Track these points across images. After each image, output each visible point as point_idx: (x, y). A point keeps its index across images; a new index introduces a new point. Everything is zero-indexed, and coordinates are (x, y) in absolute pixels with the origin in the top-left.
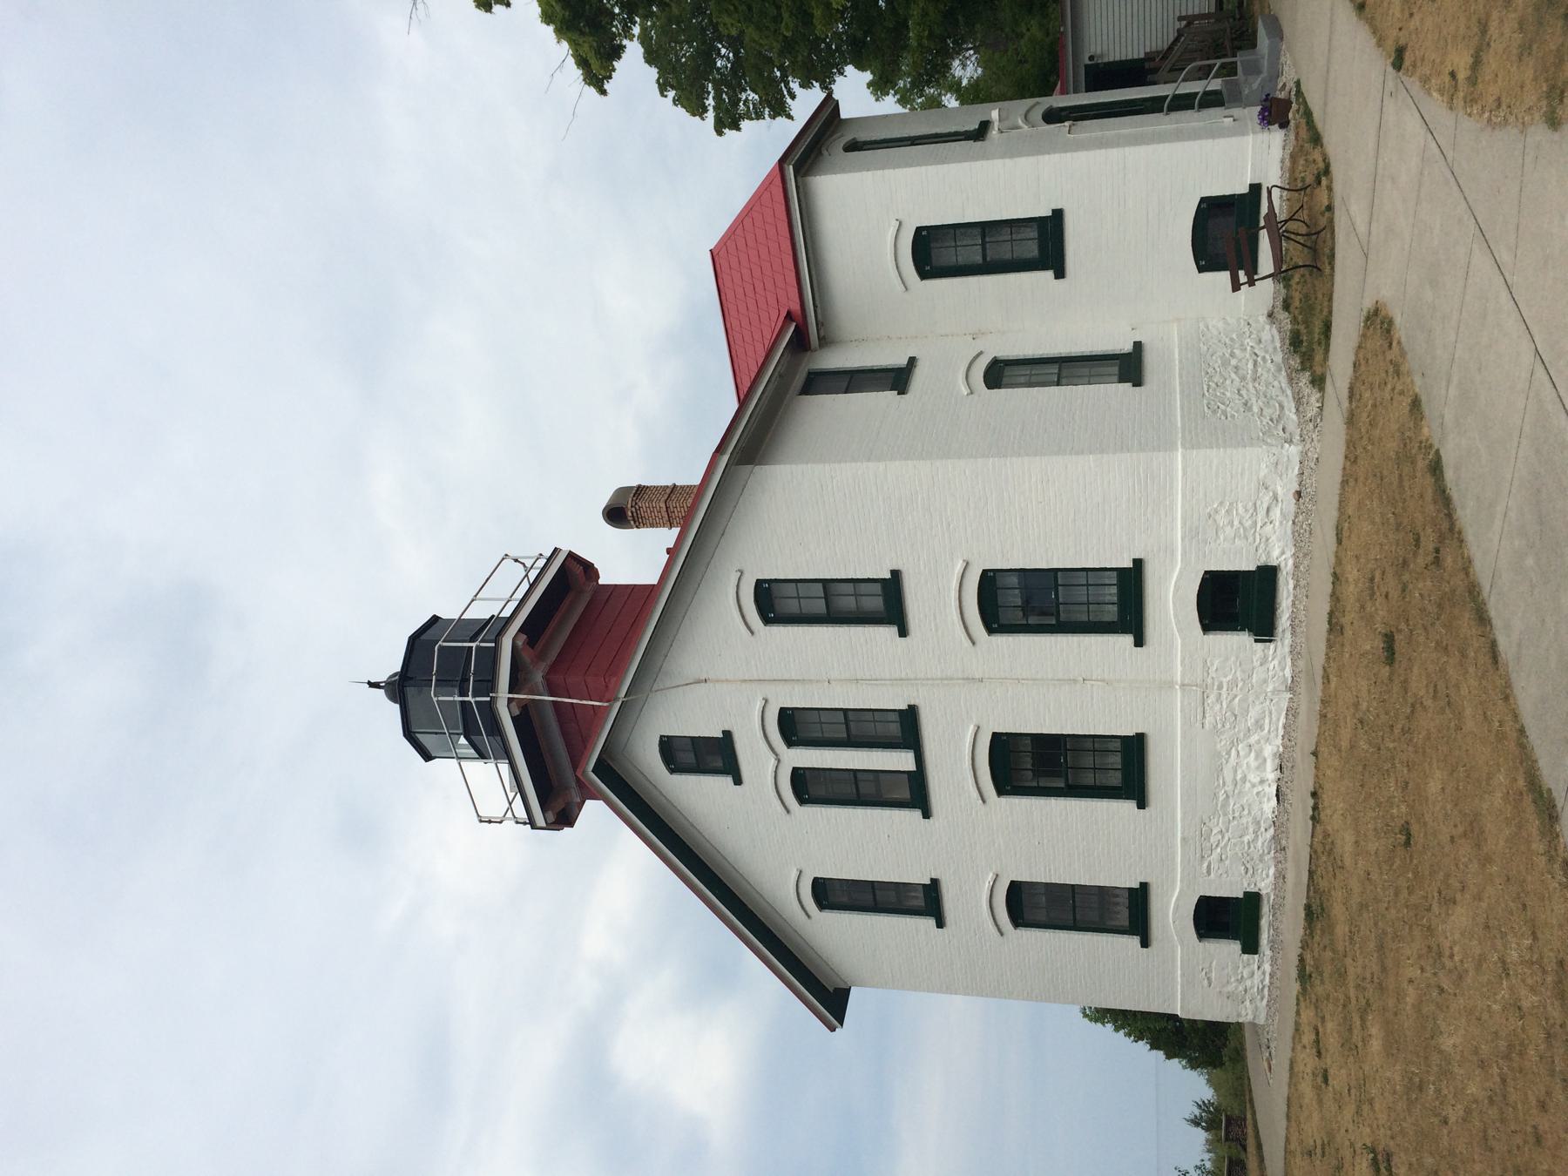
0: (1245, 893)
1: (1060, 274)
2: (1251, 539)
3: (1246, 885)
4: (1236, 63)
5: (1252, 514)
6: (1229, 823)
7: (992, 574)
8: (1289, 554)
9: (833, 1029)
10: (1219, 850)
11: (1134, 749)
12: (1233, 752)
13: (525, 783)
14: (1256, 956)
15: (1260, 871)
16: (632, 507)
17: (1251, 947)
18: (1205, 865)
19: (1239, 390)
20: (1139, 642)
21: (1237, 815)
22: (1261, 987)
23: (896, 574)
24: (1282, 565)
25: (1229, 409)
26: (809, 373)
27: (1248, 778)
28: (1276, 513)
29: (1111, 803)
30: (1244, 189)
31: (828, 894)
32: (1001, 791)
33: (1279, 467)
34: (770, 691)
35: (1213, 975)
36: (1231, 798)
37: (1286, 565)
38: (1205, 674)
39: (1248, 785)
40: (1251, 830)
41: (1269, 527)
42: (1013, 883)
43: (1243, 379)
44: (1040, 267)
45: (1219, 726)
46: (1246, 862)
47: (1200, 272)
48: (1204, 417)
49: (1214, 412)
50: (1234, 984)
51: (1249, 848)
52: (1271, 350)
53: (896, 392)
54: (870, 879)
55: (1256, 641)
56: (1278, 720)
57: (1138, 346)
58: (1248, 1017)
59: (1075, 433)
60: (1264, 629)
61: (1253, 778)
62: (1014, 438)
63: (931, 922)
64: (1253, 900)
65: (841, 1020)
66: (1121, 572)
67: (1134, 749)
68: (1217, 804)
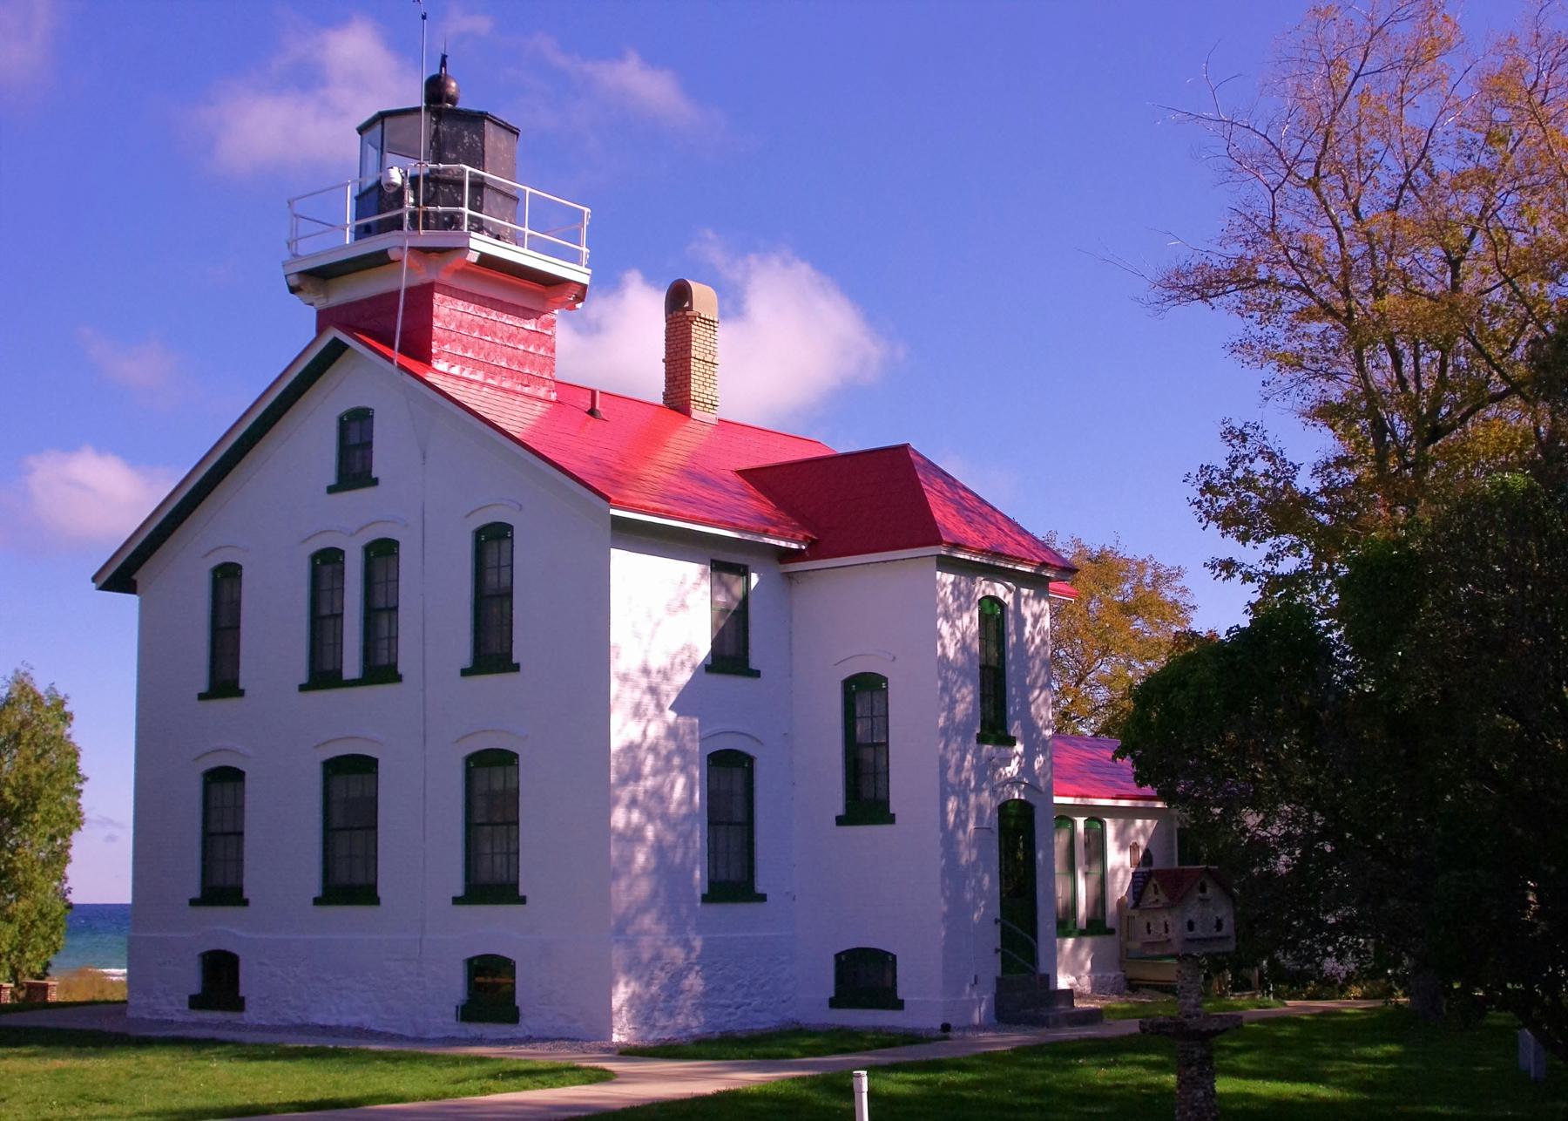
9: (94, 579)
13: (366, 349)
14: (187, 1008)
23: (375, 482)
30: (900, 996)
31: (227, 577)
54: (243, 625)
55: (457, 1007)
57: (762, 898)
64: (238, 1004)
65: (105, 587)
66: (516, 886)
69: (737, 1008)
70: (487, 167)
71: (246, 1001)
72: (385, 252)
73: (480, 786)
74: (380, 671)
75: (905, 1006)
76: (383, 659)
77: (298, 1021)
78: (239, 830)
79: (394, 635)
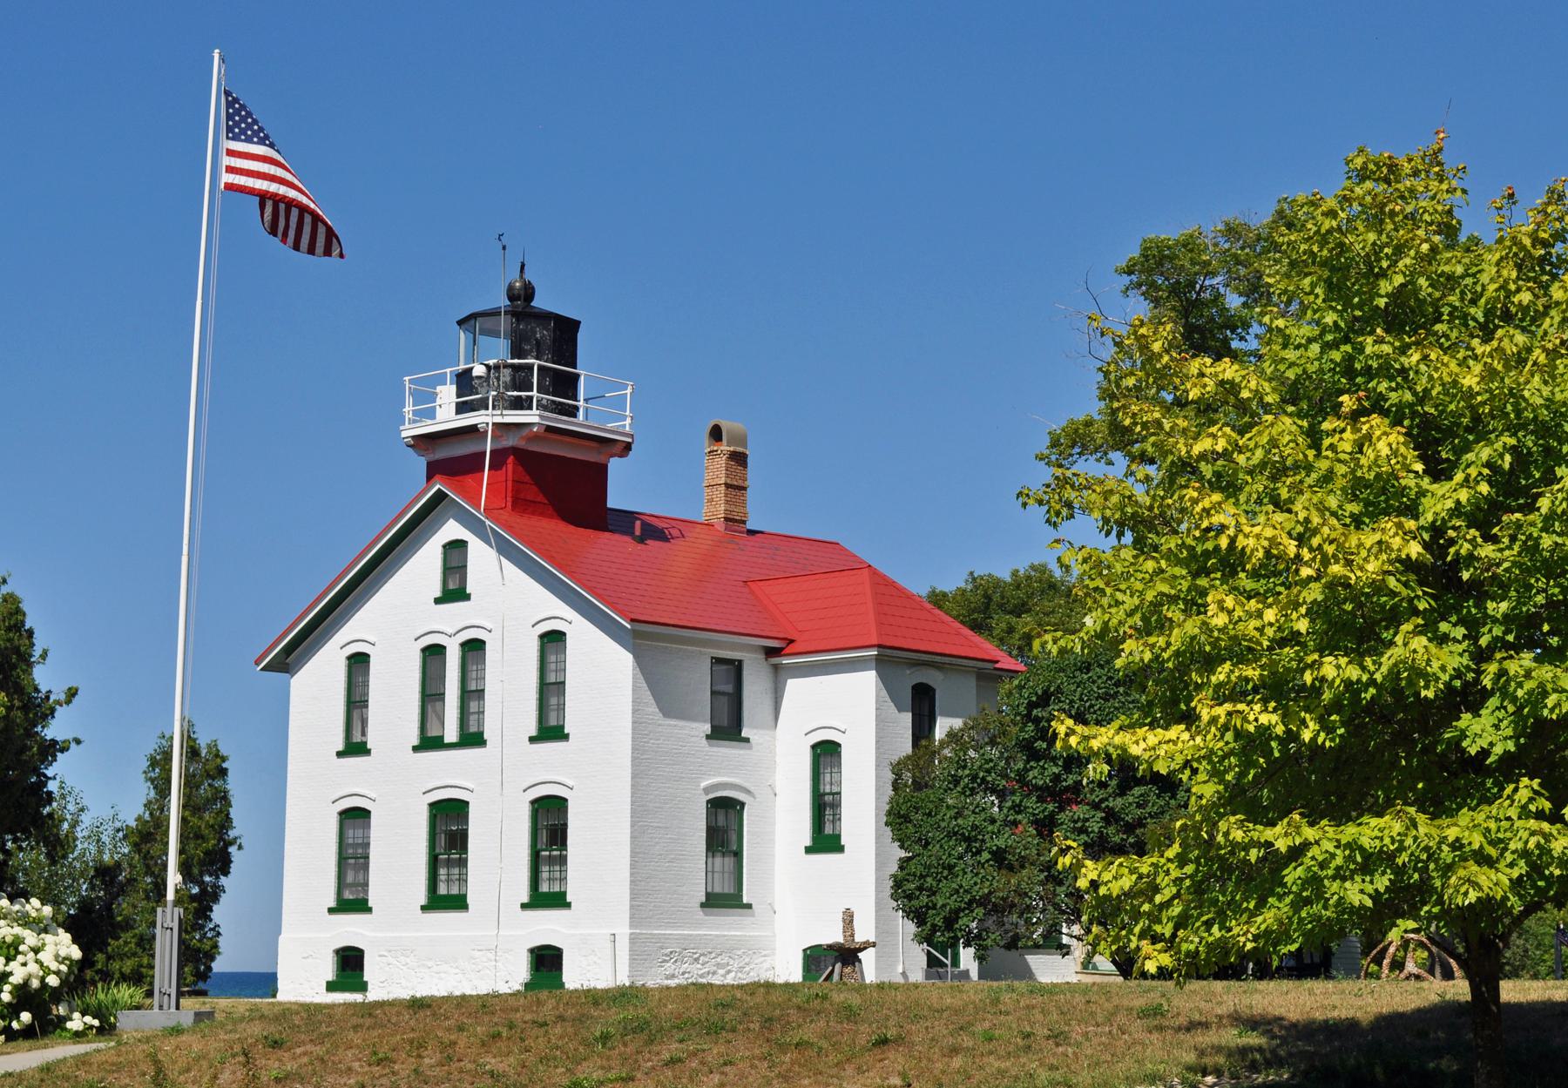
4: (487, 409)
11: (458, 903)
12: (457, 971)
17: (331, 987)
18: (385, 954)
21: (418, 974)
26: (740, 662)
31: (358, 663)
32: (433, 805)
34: (497, 633)
49: (666, 955)
63: (341, 747)
64: (362, 987)
66: (564, 894)
72: (476, 425)
74: (472, 738)
76: (357, 738)
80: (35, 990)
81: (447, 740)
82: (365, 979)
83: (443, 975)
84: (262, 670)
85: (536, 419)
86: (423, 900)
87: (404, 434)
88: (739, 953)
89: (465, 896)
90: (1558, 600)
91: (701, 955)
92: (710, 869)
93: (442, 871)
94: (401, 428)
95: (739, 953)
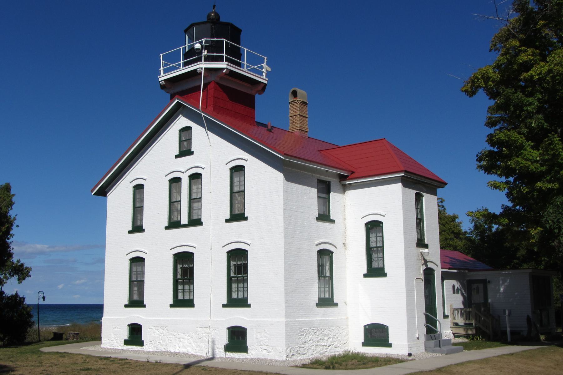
0: (144, 341)
1: (365, 276)
2: (257, 344)
3: (146, 341)
4: (202, 61)
5: (264, 344)
6: (166, 336)
7: (381, 225)
8: (252, 357)
10: (157, 332)
11: (189, 303)
15: (151, 346)
16: (297, 101)
17: (126, 342)
18: (152, 327)
19: (312, 340)
20: (224, 306)
22: (114, 346)
24: (248, 354)
25: (303, 337)
26: (329, 182)
27: (181, 343)
28: (265, 352)
29: (171, 295)
30: (390, 342)
31: (139, 188)
33: (279, 353)
35: (117, 329)
36: (174, 336)
37: (248, 356)
38: (214, 328)
39: (178, 342)
40: (164, 343)
41: (260, 350)
42: (144, 259)
43: (318, 342)
44: (368, 268)
45: (197, 333)
46: (154, 341)
47: (364, 326)
48: (300, 328)
49: (302, 332)
50: (114, 336)
51: (158, 343)
52: (331, 351)
53: (317, 216)
55: (224, 346)
56: (199, 353)
57: (336, 305)
58: (103, 341)
59: (295, 284)
60: (229, 348)
61: (181, 345)
62: (291, 262)
63: (130, 229)
64: (141, 343)
66: (246, 299)
67: (189, 303)
68: (172, 332)
69: (329, 346)
70: (197, 84)
71: (145, 342)
72: (196, 69)
73: (134, 269)
74: (195, 222)
75: (392, 345)
77: (164, 350)
78: (143, 279)
79: (199, 208)
80: (523, 109)
81: (182, 223)
82: (143, 339)
83: (181, 340)
84: (94, 194)
85: (225, 66)
86: (171, 302)
87: (160, 80)
88: (333, 328)
89: (192, 300)
90: (555, 188)
91: (317, 330)
92: (319, 287)
93: (180, 287)
94: (159, 77)
95: (333, 328)
